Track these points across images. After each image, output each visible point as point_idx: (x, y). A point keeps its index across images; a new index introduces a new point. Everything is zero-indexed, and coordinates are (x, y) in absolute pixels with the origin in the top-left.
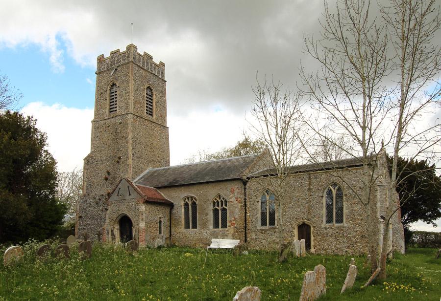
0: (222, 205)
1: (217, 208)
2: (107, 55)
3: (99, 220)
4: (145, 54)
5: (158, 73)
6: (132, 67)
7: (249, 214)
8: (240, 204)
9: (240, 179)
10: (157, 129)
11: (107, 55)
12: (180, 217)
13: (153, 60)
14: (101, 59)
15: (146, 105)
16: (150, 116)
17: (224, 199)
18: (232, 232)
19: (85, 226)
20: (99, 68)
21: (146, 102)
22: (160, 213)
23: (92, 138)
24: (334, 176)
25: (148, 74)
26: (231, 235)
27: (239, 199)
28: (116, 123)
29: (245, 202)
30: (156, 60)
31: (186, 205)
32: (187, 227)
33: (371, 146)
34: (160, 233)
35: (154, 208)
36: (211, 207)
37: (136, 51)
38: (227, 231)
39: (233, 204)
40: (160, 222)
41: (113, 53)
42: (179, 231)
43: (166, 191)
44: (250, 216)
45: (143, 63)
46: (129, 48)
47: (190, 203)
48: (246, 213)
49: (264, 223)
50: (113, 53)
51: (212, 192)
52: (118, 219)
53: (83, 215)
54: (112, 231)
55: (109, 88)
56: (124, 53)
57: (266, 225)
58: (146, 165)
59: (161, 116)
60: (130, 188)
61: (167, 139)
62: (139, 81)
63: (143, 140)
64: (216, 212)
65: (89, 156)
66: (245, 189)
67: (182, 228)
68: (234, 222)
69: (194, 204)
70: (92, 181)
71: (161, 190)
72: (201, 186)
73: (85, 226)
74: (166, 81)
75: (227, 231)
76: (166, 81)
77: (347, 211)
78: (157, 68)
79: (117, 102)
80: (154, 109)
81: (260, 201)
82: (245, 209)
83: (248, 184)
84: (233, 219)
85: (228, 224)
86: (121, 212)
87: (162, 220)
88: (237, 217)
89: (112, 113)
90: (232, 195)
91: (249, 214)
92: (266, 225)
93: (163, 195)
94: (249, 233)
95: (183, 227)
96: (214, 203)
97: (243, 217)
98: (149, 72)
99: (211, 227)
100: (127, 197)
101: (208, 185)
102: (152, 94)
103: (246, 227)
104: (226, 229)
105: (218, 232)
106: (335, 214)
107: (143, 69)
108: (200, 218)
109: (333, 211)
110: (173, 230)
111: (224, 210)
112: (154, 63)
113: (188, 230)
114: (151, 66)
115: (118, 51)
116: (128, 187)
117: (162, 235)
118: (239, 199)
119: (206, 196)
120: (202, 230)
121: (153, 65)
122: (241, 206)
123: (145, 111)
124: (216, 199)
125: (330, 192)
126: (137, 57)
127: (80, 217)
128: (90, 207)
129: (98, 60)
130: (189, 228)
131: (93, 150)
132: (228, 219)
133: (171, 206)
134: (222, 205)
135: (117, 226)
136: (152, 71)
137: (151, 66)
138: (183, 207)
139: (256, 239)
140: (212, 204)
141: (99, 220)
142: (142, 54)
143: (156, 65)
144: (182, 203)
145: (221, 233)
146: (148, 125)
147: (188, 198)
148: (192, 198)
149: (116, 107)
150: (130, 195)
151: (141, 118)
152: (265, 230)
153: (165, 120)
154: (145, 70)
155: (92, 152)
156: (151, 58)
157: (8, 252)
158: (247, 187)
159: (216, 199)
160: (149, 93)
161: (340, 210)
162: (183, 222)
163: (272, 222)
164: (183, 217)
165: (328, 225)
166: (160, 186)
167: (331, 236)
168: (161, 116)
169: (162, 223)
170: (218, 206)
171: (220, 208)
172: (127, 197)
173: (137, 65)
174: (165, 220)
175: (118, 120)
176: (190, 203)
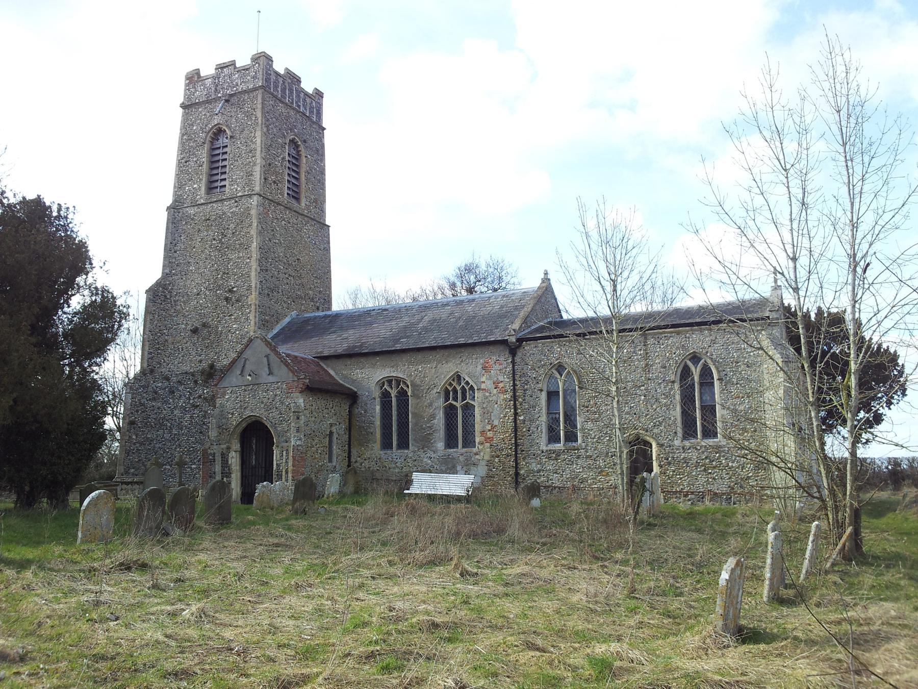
0: (464, 398)
1: (454, 403)
2: (207, 70)
3: (174, 432)
4: (289, 72)
5: (311, 112)
6: (263, 99)
7: (522, 418)
8: (502, 396)
9: (504, 342)
10: (308, 229)
11: (207, 70)
12: (373, 423)
13: (302, 85)
14: (194, 78)
15: (286, 178)
16: (294, 201)
17: (467, 383)
18: (487, 457)
19: (142, 444)
20: (187, 97)
21: (287, 171)
22: (331, 416)
23: (166, 245)
24: (697, 341)
25: (292, 113)
26: (484, 463)
27: (501, 385)
28: (224, 213)
29: (514, 391)
30: (308, 86)
31: (386, 395)
32: (387, 444)
33: (813, 287)
34: (330, 461)
35: (320, 403)
36: (441, 402)
37: (271, 66)
38: (476, 454)
39: (487, 394)
40: (331, 433)
41: (221, 67)
42: (367, 455)
43: (340, 364)
44: (524, 421)
45: (284, 90)
46: (256, 59)
47: (393, 393)
48: (516, 414)
49: (553, 437)
50: (222, 68)
51: (436, 373)
52: (241, 429)
53: (139, 419)
54: (223, 455)
55: (208, 139)
56: (246, 69)
57: (558, 440)
58: (285, 305)
59: (316, 201)
60: (273, 357)
61: (327, 250)
62: (276, 126)
63: (280, 251)
64: (450, 412)
65: (158, 284)
66: (513, 362)
67: (375, 449)
68: (490, 434)
69: (403, 394)
70: (161, 340)
71: (328, 362)
72: (420, 356)
73: (142, 444)
74: (324, 129)
75: (476, 454)
76: (324, 129)
77: (725, 412)
78: (308, 100)
79: (227, 170)
80: (303, 186)
81: (545, 389)
82: (515, 405)
83: (519, 354)
84: (489, 427)
85: (477, 440)
86: (248, 413)
87: (334, 429)
88: (496, 423)
89: (215, 191)
90: (488, 378)
91: (522, 418)
92: (559, 441)
93: (332, 373)
94: (524, 459)
95: (377, 445)
96: (447, 392)
97: (510, 425)
98: (294, 109)
99: (441, 445)
100: (265, 378)
101: (434, 353)
102: (299, 155)
103: (516, 445)
104: (475, 450)
105: (455, 455)
106: (697, 419)
107: (283, 103)
108: (416, 424)
109: (398, 406)
110: (354, 452)
111: (468, 409)
112: (303, 91)
113: (389, 452)
114: (298, 96)
115: (233, 63)
116: (267, 356)
117: (334, 464)
118: (501, 385)
119: (431, 376)
120: (421, 453)
121: (302, 95)
122: (505, 400)
123: (286, 191)
124: (451, 384)
125: (686, 373)
126: (273, 77)
127: (132, 423)
128: (154, 399)
129: (187, 79)
130: (391, 448)
131: (167, 271)
132: (478, 428)
133: (352, 397)
134: (464, 398)
135: (236, 446)
136: (299, 106)
137: (298, 96)
138: (378, 400)
139: (539, 471)
140: (442, 395)
141: (174, 432)
142: (282, 72)
143: (306, 94)
144: (377, 394)
145: (462, 459)
146: (291, 221)
147: (390, 382)
148: (398, 381)
149: (225, 179)
150: (271, 373)
151: (278, 204)
152: (558, 454)
153: (322, 211)
154: (286, 104)
155: (165, 275)
156: (298, 81)
157: (89, 503)
158: (517, 359)
159: (451, 384)
160: (293, 152)
161: (709, 410)
162: (441, 433)
163: (571, 437)
164: (378, 423)
165: (687, 443)
166: (326, 353)
167: (697, 465)
168: (316, 201)
169: (335, 436)
170: (455, 399)
171: (458, 404)
172: (265, 378)
173: (272, 94)
174: (340, 430)
175: (228, 208)
176: (393, 393)
